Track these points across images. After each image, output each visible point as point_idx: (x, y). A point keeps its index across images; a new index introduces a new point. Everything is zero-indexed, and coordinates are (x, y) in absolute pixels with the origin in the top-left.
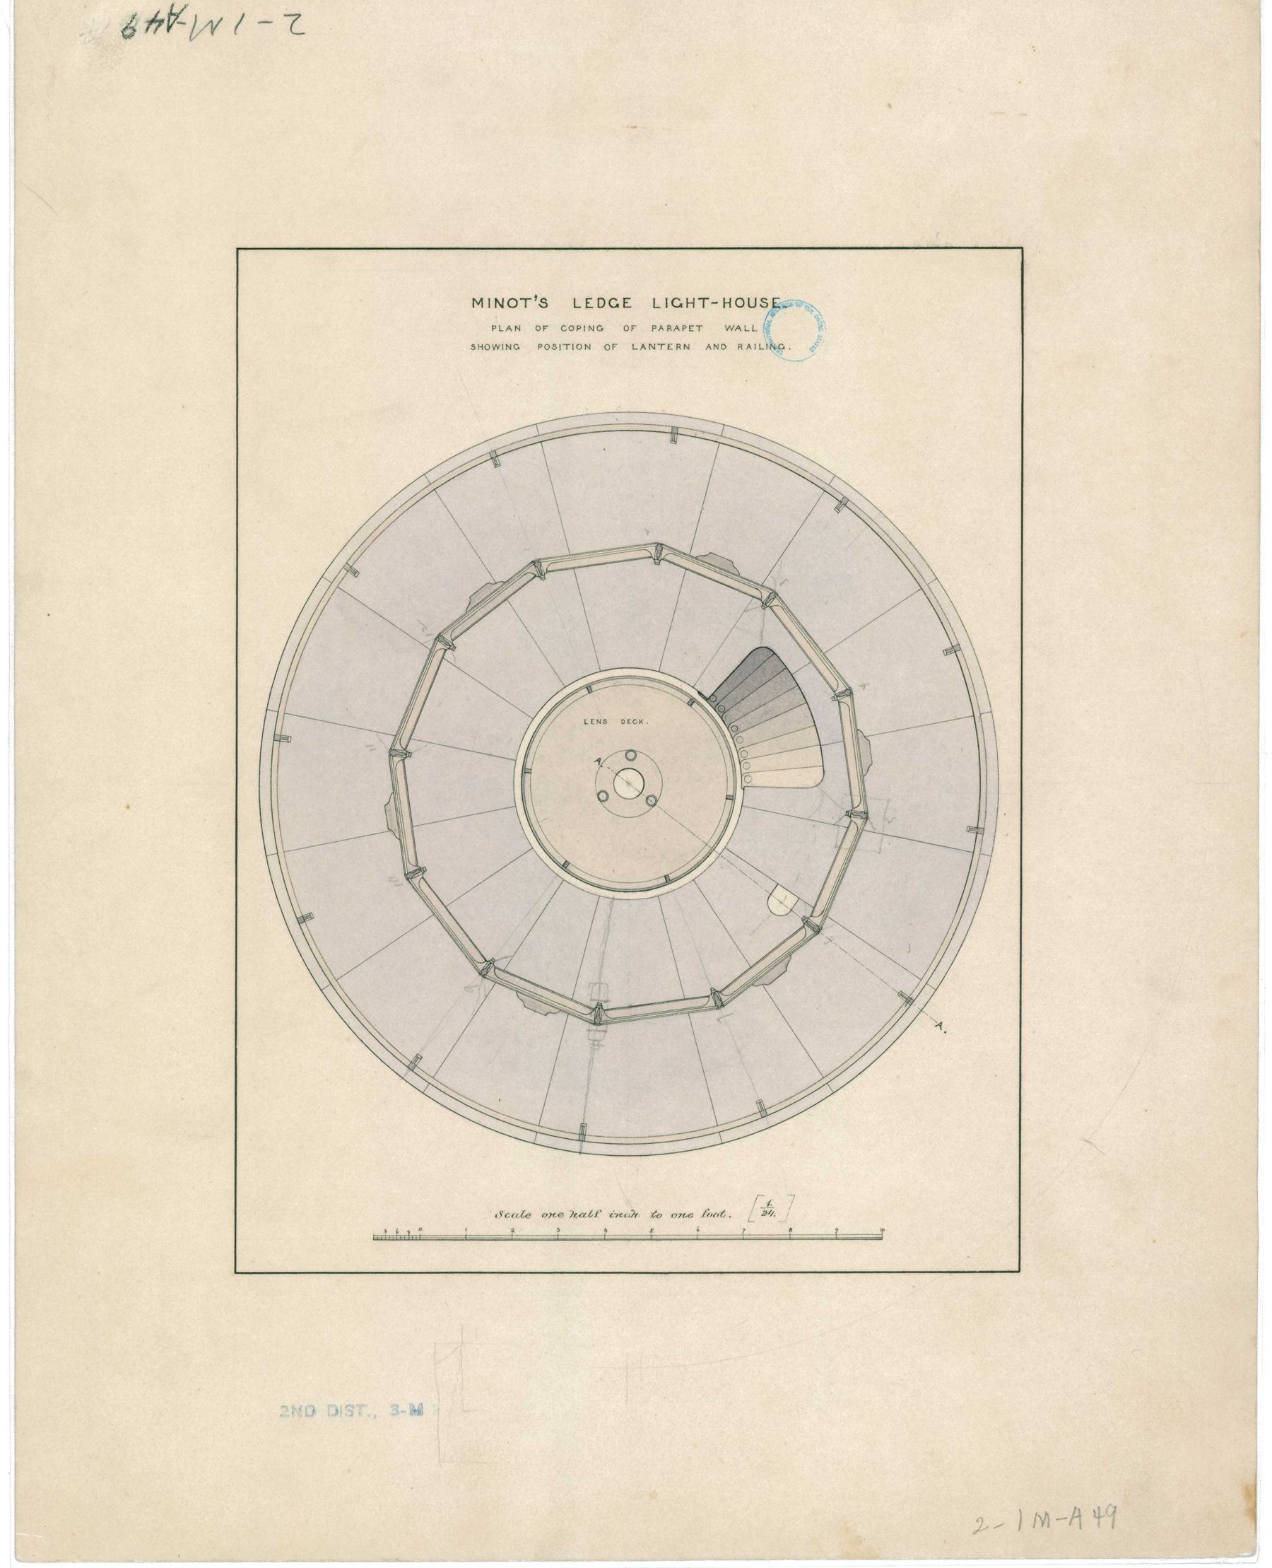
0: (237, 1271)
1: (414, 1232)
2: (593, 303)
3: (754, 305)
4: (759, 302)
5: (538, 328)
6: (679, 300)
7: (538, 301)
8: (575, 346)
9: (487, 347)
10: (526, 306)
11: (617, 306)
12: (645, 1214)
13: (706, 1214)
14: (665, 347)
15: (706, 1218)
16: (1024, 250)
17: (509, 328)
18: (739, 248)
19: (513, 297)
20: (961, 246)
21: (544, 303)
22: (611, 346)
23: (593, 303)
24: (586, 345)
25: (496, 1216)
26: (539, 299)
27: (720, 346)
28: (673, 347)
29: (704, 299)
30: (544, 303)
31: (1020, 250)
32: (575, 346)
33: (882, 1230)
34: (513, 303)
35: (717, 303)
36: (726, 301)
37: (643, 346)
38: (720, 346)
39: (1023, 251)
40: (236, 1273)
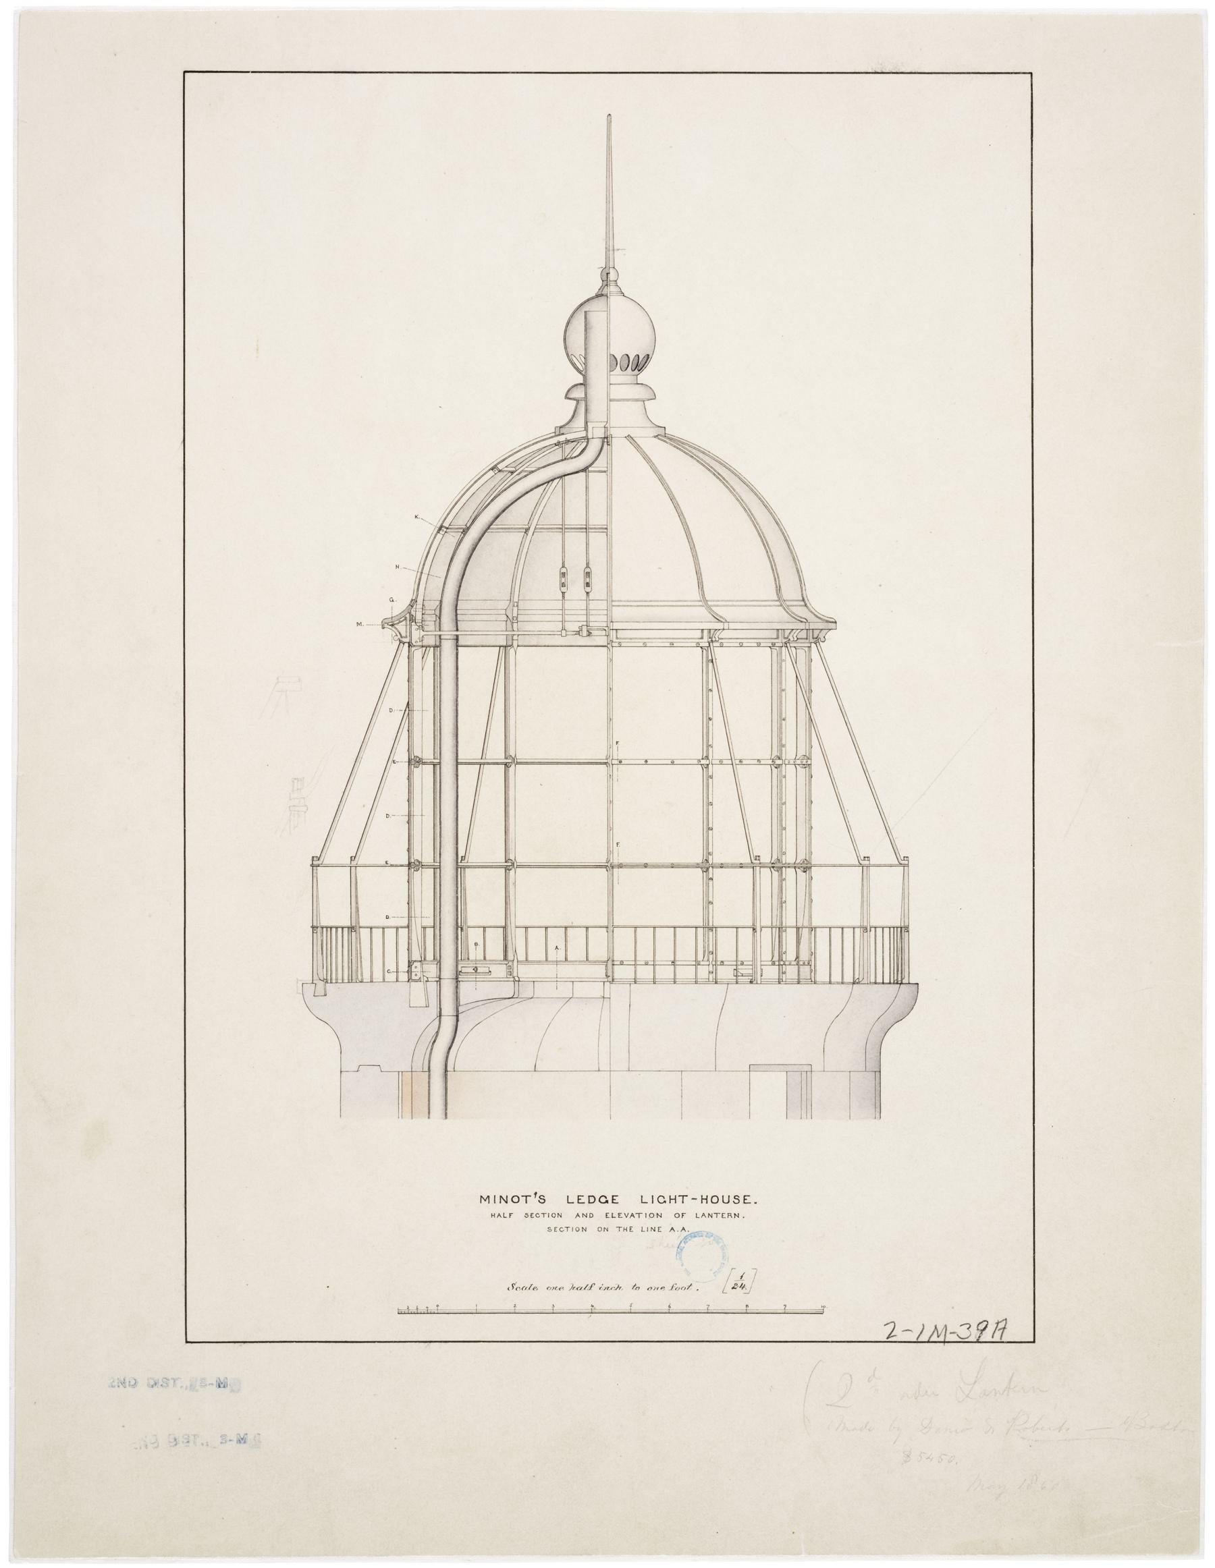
0: (188, 1340)
2: (584, 1199)
4: (732, 1199)
5: (600, 1229)
6: (606, 1198)
7: (537, 1198)
8: (550, 1215)
11: (607, 1202)
12: (613, 1230)
13: (674, 1288)
14: (720, 1216)
17: (704, 1215)
18: (657, 73)
19: (516, 1194)
20: (184, 1255)
23: (584, 1199)
24: (735, 1214)
25: (508, 1289)
27: (588, 1215)
28: (726, 1216)
29: (683, 1196)
30: (542, 1200)
31: (1032, 1340)
32: (550, 1215)
34: (515, 1199)
35: (693, 1199)
36: (674, 1201)
37: (704, 1215)
38: (588, 1215)
40: (1031, 73)
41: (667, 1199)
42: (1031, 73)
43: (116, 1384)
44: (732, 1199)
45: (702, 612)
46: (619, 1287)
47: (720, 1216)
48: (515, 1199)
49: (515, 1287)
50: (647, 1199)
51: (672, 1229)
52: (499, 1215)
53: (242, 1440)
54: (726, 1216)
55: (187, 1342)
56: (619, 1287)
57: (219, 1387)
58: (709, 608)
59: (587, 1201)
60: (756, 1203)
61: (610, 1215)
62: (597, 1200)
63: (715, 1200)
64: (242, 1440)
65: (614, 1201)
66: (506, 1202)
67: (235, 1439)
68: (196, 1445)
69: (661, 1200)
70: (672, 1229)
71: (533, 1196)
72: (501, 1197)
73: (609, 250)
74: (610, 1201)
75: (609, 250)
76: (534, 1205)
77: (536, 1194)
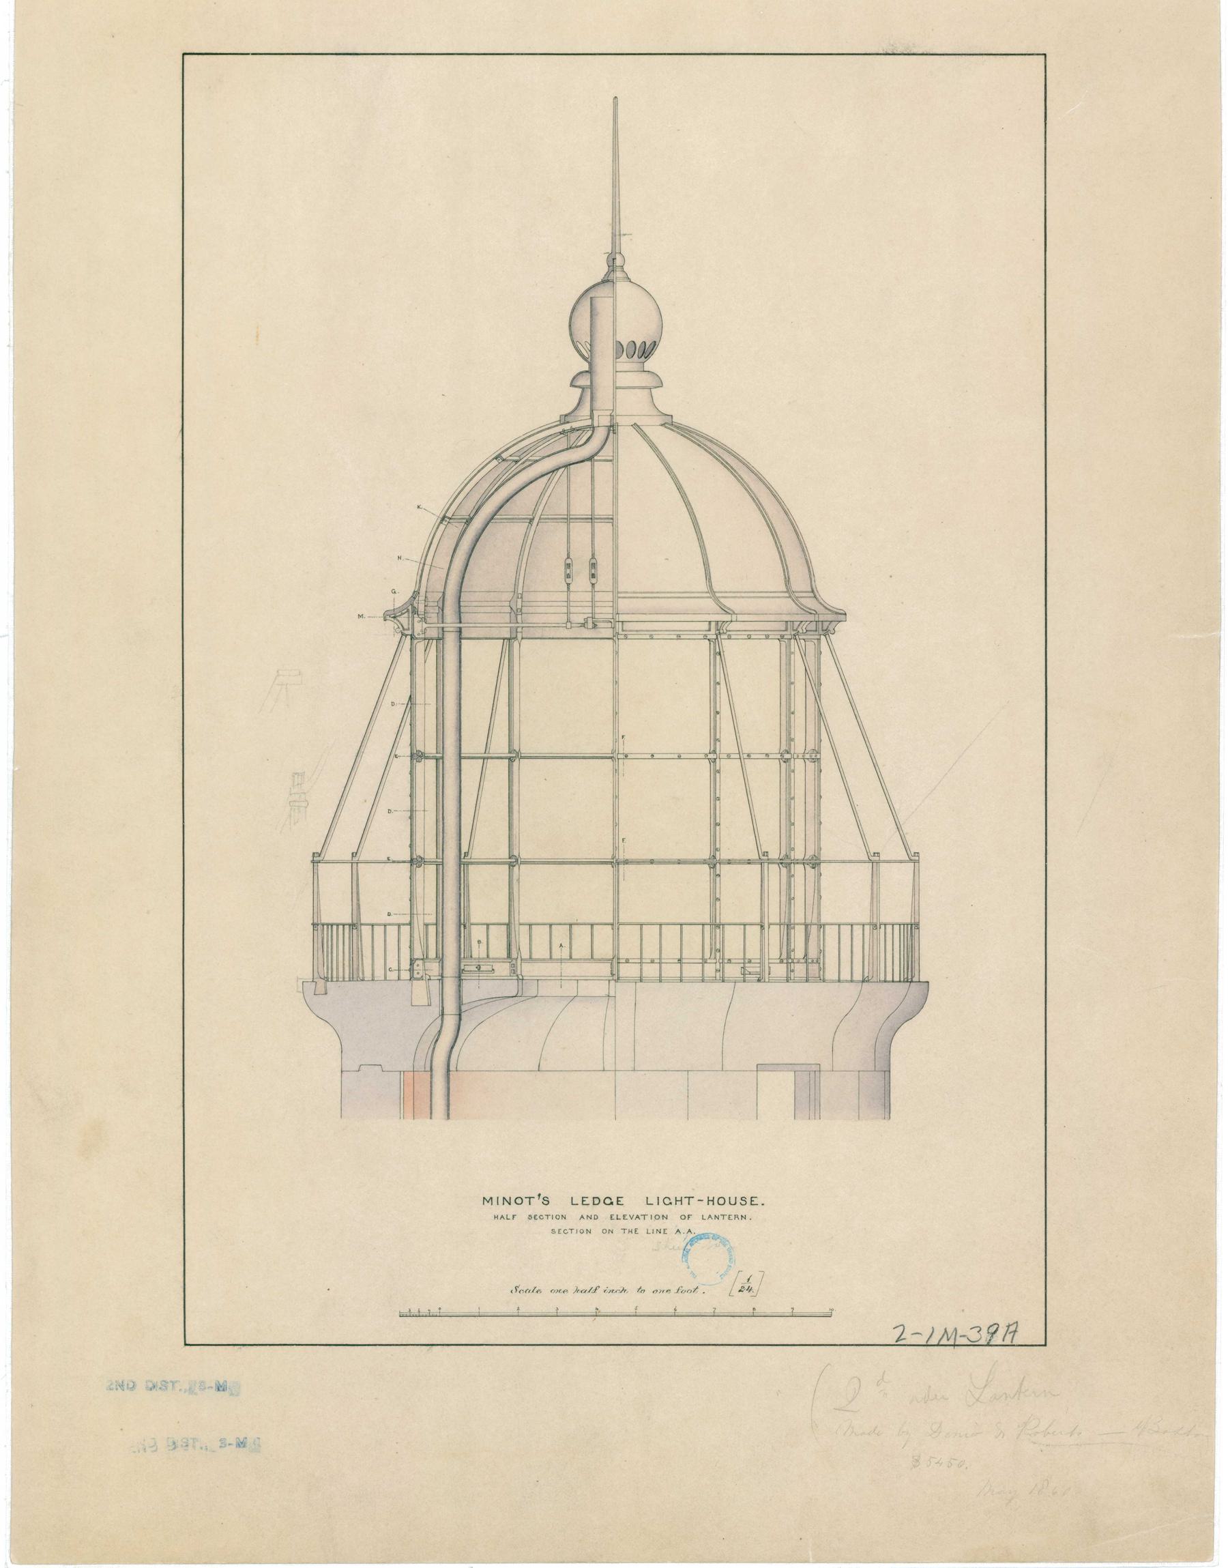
0: (187, 1343)
1: (435, 1310)
2: (589, 1201)
3: (734, 1203)
4: (739, 1200)
6: (670, 1199)
8: (554, 1216)
9: (657, 1217)
10: (689, 1204)
11: (612, 1203)
14: (726, 1218)
15: (680, 1294)
16: (185, 52)
17: (710, 1216)
21: (546, 1201)
22: (687, 1216)
23: (589, 1201)
26: (542, 1197)
27: (593, 1216)
28: (732, 1217)
30: (546, 1201)
32: (554, 1216)
33: (832, 1310)
34: (519, 1201)
37: (582, 1217)
38: (593, 1216)
39: (185, 1341)
40: (1045, 1345)
41: (673, 1201)
42: (1045, 55)
43: (114, 1386)
44: (739, 1200)
45: (709, 604)
46: (624, 1290)
47: (726, 1218)
48: (519, 1201)
49: (518, 1290)
50: (653, 1200)
51: (678, 1231)
52: (502, 1217)
53: (220, 1388)
54: (732, 1217)
55: (186, 1345)
56: (624, 1290)
57: (219, 1390)
58: (717, 600)
59: (591, 1203)
60: (763, 1204)
61: (614, 1217)
62: (602, 1201)
63: (721, 1201)
64: (220, 1388)
65: (619, 1203)
66: (510, 1204)
67: (235, 1443)
68: (195, 1449)
69: (667, 1201)
70: (678, 1231)
71: (537, 1197)
72: (504, 1198)
73: (616, 236)
74: (615, 1203)
75: (616, 236)
76: (537, 1207)
77: (539, 1195)
